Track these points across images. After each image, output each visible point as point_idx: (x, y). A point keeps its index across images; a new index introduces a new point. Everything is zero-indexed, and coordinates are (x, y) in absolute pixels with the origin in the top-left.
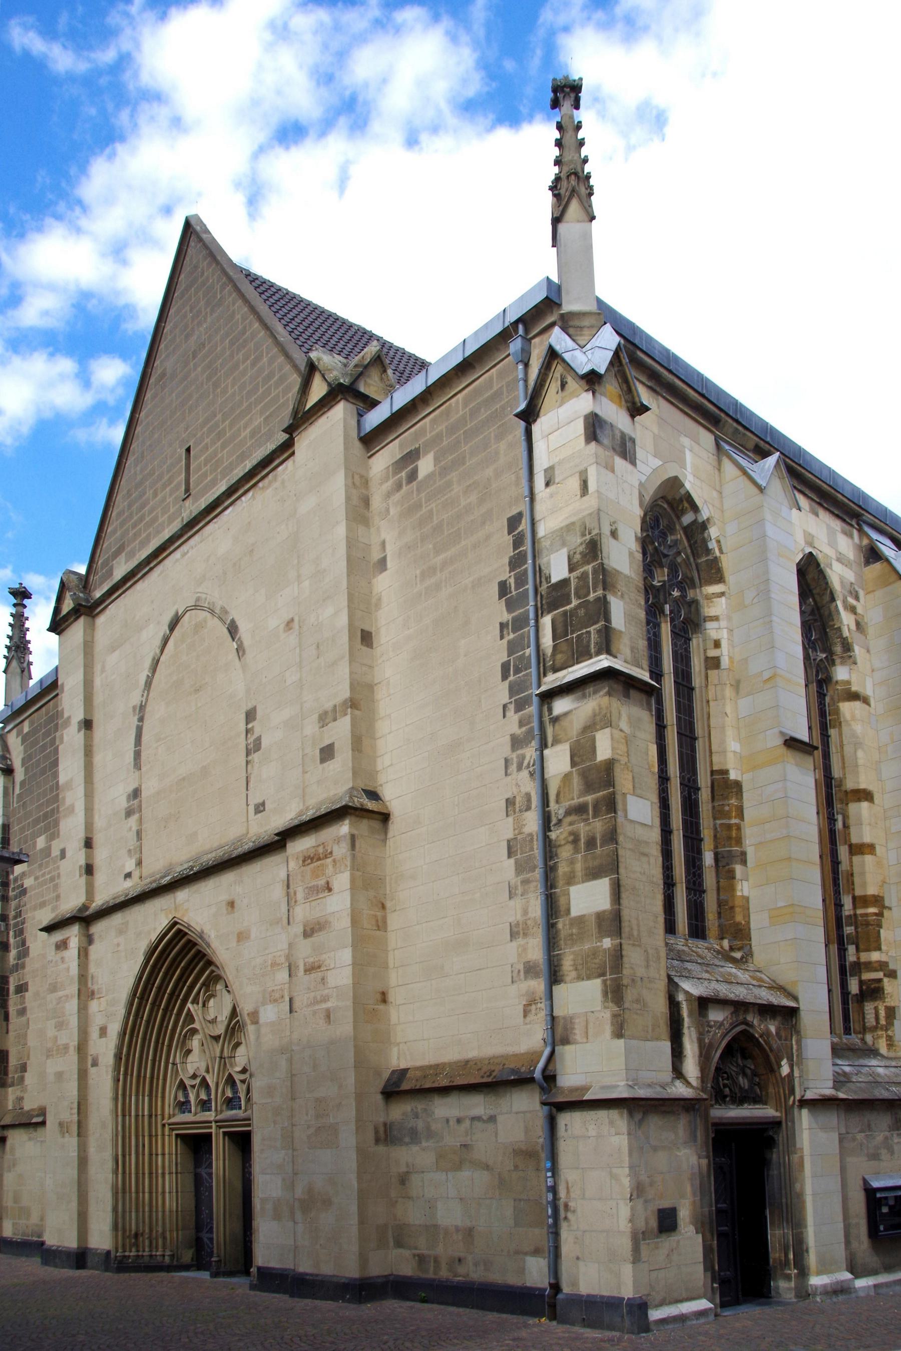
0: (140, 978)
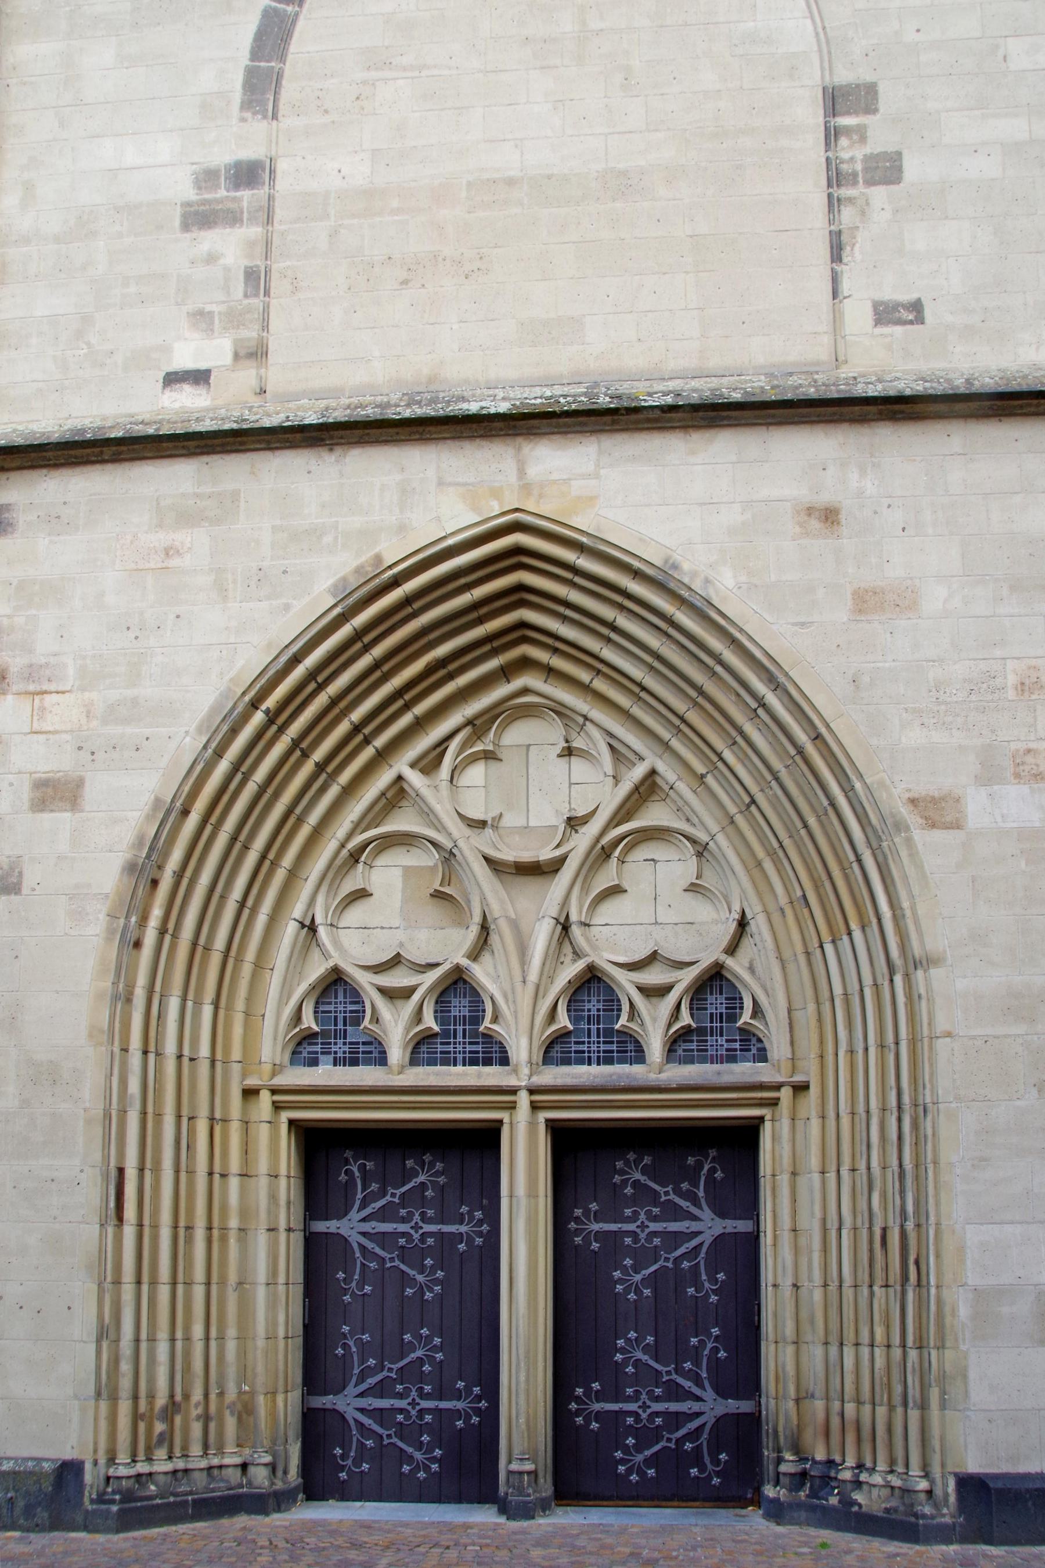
0: (296, 660)
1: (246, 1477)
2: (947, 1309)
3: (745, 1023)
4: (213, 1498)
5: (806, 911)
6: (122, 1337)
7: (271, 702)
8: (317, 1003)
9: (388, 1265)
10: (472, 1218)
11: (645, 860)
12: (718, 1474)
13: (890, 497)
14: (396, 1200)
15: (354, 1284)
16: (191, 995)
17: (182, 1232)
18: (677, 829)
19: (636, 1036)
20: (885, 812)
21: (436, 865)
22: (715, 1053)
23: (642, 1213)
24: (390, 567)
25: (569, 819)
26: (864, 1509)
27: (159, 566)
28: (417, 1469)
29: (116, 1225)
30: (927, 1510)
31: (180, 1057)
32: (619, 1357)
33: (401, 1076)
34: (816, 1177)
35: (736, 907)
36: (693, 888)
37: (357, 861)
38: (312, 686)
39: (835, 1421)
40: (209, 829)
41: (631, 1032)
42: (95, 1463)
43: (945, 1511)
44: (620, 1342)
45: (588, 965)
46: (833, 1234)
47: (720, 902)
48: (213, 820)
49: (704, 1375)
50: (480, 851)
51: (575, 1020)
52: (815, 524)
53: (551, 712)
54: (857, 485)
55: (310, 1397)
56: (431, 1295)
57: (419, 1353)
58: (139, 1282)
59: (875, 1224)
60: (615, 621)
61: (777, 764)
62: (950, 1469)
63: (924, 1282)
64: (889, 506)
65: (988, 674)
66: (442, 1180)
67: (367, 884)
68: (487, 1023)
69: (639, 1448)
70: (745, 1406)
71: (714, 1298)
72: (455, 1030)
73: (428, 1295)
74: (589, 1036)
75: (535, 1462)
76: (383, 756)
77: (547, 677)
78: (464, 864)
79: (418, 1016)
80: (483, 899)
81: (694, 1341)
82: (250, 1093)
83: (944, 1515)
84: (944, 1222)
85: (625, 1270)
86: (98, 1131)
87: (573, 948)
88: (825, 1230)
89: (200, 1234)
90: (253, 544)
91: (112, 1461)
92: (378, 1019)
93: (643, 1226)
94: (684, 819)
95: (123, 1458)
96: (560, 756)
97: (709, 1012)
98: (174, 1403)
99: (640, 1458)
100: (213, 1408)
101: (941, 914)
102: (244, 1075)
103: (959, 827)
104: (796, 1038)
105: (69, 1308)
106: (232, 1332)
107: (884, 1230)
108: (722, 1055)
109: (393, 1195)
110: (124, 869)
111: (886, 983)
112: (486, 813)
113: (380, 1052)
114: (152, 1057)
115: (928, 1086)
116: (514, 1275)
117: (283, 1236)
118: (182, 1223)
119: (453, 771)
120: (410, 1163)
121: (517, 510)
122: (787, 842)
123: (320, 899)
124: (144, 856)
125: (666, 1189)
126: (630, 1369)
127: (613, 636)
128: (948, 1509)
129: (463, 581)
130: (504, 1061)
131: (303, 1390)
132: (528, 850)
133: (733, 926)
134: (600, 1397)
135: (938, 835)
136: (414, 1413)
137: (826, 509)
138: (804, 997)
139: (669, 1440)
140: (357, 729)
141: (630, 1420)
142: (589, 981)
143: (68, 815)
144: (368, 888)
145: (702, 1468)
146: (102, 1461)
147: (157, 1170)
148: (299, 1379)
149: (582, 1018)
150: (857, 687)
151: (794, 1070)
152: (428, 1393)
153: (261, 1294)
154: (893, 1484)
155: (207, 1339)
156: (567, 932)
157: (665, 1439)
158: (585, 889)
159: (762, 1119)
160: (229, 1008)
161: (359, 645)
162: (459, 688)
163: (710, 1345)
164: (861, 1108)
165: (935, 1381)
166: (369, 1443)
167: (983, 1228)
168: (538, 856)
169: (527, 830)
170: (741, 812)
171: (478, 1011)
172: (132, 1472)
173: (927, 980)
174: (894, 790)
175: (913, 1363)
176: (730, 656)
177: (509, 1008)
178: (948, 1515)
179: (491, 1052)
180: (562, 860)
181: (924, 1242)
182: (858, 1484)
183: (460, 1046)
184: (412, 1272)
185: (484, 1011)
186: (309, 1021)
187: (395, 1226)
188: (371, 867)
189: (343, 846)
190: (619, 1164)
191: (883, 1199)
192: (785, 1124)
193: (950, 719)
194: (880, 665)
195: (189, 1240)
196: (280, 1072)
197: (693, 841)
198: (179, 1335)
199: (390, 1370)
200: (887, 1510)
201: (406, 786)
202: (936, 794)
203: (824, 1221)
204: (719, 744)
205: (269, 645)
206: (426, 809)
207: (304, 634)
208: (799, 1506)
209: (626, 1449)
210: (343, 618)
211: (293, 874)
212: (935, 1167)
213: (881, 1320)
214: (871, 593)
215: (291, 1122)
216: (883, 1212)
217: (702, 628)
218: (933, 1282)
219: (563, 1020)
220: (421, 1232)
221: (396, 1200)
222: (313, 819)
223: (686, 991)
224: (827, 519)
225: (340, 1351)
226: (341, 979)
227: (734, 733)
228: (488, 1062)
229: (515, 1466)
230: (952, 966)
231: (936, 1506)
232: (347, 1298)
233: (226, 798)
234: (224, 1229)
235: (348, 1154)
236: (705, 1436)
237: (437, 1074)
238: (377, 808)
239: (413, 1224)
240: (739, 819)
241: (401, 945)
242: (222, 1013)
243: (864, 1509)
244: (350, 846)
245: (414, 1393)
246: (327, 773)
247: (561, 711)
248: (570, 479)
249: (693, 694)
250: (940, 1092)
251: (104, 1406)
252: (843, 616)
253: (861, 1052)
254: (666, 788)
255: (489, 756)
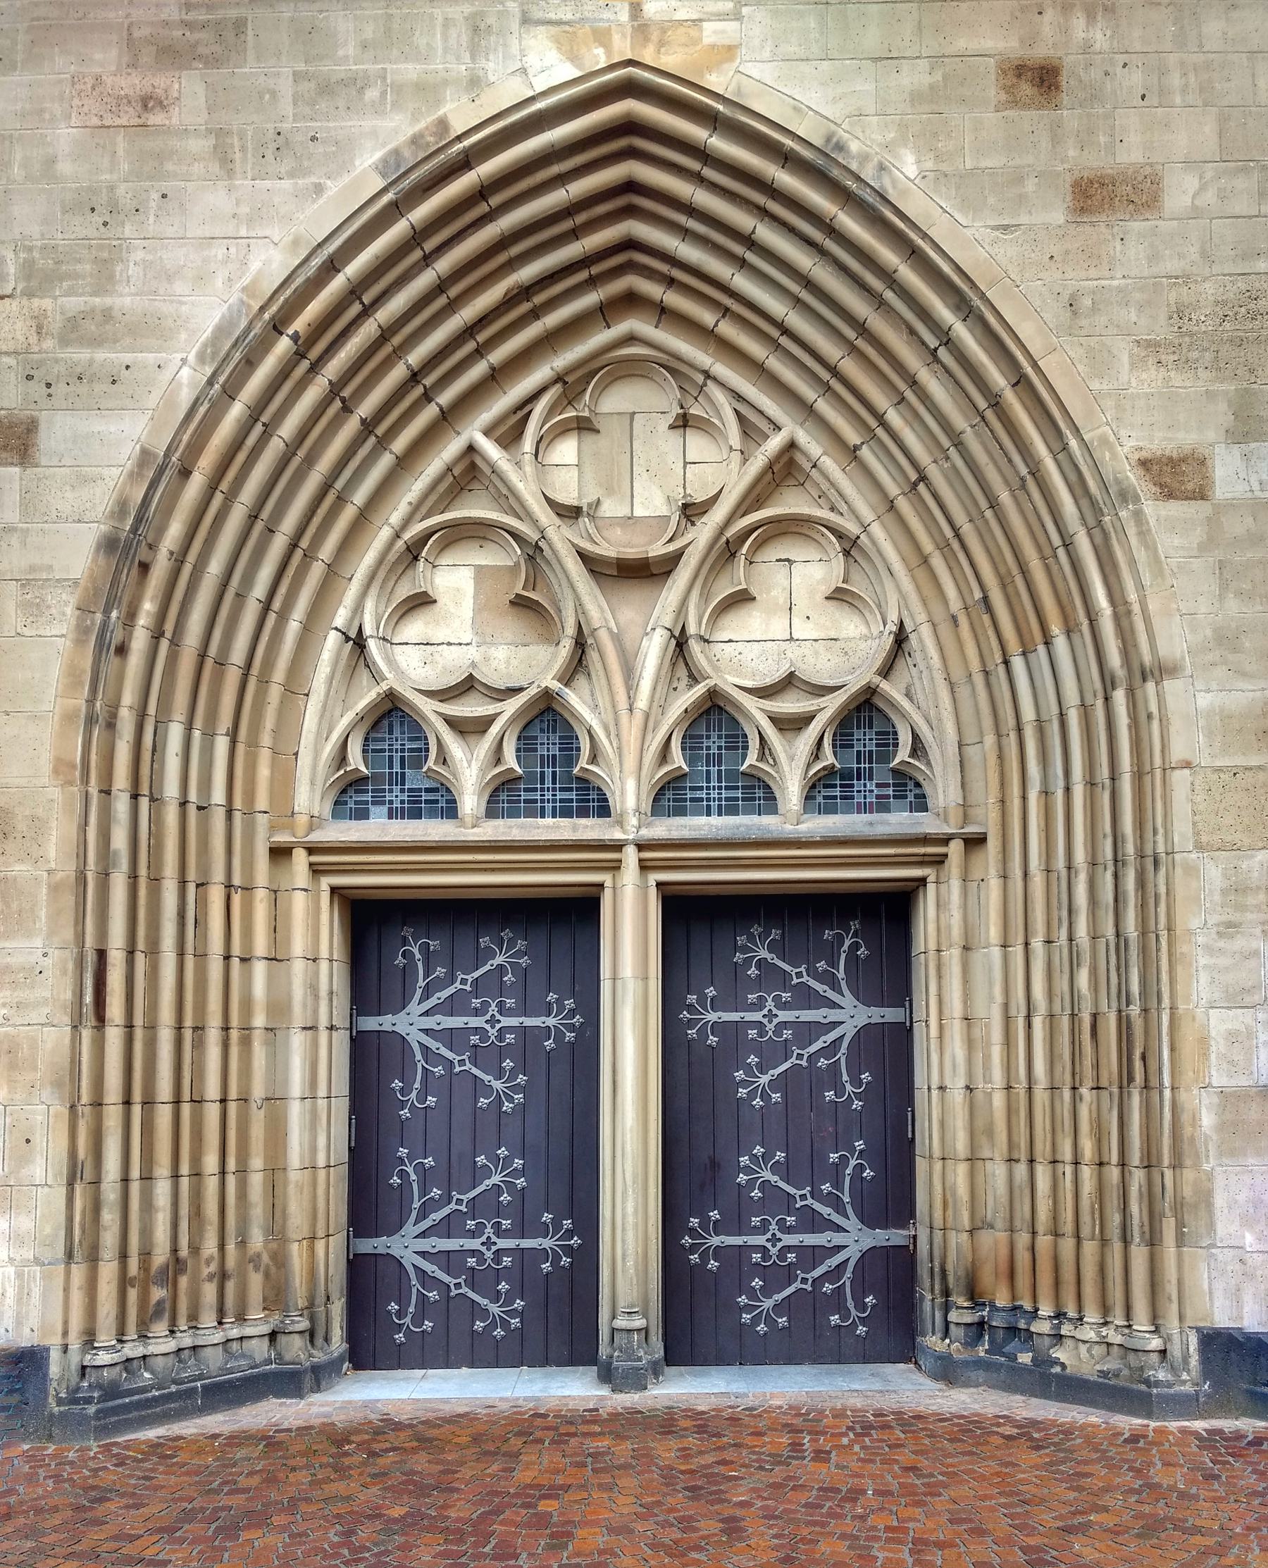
0: (332, 267)
1: (275, 1349)
2: (1185, 1118)
3: (903, 762)
4: (229, 1382)
5: (986, 618)
6: (103, 1176)
7: (300, 324)
8: (366, 739)
9: (458, 1069)
10: (561, 1008)
11: (777, 561)
12: (863, 1321)
13: (1127, 52)
14: (468, 988)
15: (413, 1095)
16: (198, 722)
17: (188, 1034)
18: (820, 518)
19: (766, 779)
20: (1109, 477)
21: (517, 564)
22: (863, 800)
23: (770, 1000)
24: (459, 138)
25: (685, 506)
26: (1068, 1371)
27: (136, 121)
28: (493, 1326)
29: (94, 1027)
30: (1162, 1375)
31: (184, 804)
32: (742, 1178)
33: (476, 830)
34: (996, 952)
35: (893, 617)
36: (839, 596)
37: (416, 558)
38: (356, 308)
39: (1023, 1258)
40: (218, 499)
41: (761, 775)
42: (65, 1349)
43: (1185, 1376)
44: (744, 1160)
45: (709, 690)
46: (1021, 1023)
47: (872, 611)
48: (224, 486)
49: (847, 1199)
50: (573, 545)
51: (691, 761)
52: (1026, 89)
53: (661, 369)
54: (1083, 35)
55: (357, 1240)
56: (511, 1105)
57: (496, 1179)
58: (127, 1103)
59: (1083, 1009)
60: (753, 232)
61: (959, 421)
62: (1189, 1323)
63: (1154, 1082)
64: (1125, 65)
65: (1248, 294)
66: (524, 961)
67: (429, 585)
68: (583, 762)
69: (767, 1291)
70: (896, 1237)
71: (857, 1104)
72: (542, 773)
73: (507, 1106)
74: (708, 781)
75: (645, 1316)
76: (448, 418)
77: (659, 321)
78: (554, 562)
79: (497, 755)
80: (579, 606)
81: (834, 1157)
82: (280, 853)
83: (1184, 1382)
84: (1182, 1007)
85: (748, 1069)
86: (69, 900)
87: (689, 670)
88: (1007, 1019)
89: (213, 1036)
90: (267, 96)
91: (89, 1341)
92: (445, 759)
93: (770, 1016)
94: (827, 507)
95: (105, 1337)
96: (672, 427)
97: (855, 749)
98: (177, 1260)
99: (768, 1304)
100: (231, 1263)
101: (1178, 610)
102: (273, 829)
103: (1203, 497)
104: (967, 779)
105: (28, 1141)
106: (257, 1162)
107: (1095, 1016)
108: (871, 803)
109: (464, 982)
110: (98, 550)
111: (1100, 703)
112: (580, 497)
113: (448, 802)
114: (144, 803)
115: (1161, 831)
116: (619, 1078)
117: (323, 1036)
118: (188, 1022)
119: (538, 443)
120: (484, 941)
121: (630, 63)
122: (967, 529)
123: (370, 605)
124: (128, 528)
125: (798, 970)
126: (756, 1193)
127: (750, 257)
128: (1189, 1375)
129: (555, 169)
130: (604, 810)
131: (348, 1231)
132: (632, 547)
133: (888, 641)
134: (719, 1229)
135: (1175, 508)
136: (489, 1255)
137: (1042, 68)
138: (980, 727)
139: (804, 1281)
140: (415, 377)
141: (756, 1257)
142: (707, 712)
143: (17, 470)
144: (430, 593)
145: (845, 1315)
146: (75, 1345)
147: (154, 951)
148: (344, 1219)
149: (699, 758)
150: (1075, 313)
151: (966, 819)
152: (506, 1230)
153: (296, 1113)
154: (1110, 1340)
155: (223, 1172)
156: (681, 650)
157: (799, 1279)
158: (705, 597)
159: (923, 881)
160: (253, 743)
161: (417, 254)
162: (546, 331)
163: (853, 1162)
164: (1060, 863)
165: (1171, 1209)
166: (433, 1295)
167: (1231, 1013)
168: (647, 552)
169: (631, 522)
170: (904, 494)
171: (571, 749)
172: (116, 1357)
173: (1160, 697)
174: (1120, 448)
175: (1140, 1187)
176: (908, 275)
177: (611, 744)
178: (1189, 1380)
179: (588, 801)
180: (674, 559)
181: (1154, 1032)
182: (1058, 1338)
183: (550, 795)
184: (486, 1078)
185: (578, 749)
186: (356, 760)
187: (465, 1019)
188: (434, 567)
189: (397, 536)
190: (741, 940)
191: (1093, 978)
192: (955, 884)
193: (1195, 354)
194: (1104, 283)
195: (199, 1044)
196: (320, 827)
197: (840, 535)
198: (185, 1169)
199: (459, 1202)
200: (1103, 1374)
201: (479, 462)
202: (1175, 455)
203: (1006, 1006)
204: (880, 399)
205: (296, 243)
206: (505, 491)
207: (345, 227)
208: (979, 1364)
209: (752, 1294)
210: (396, 210)
211: (333, 573)
212: (1169, 935)
213: (1091, 1130)
214: (1096, 186)
215: (334, 890)
216: (1093, 995)
217: (874, 236)
218: (1167, 1081)
219: (678, 760)
220: (498, 1026)
221: (468, 988)
222: (360, 496)
223: (830, 722)
224: (1042, 81)
225: (396, 1180)
226: (397, 709)
227: (902, 386)
228: (583, 813)
229: (621, 1323)
230: (1192, 676)
231: (1173, 1369)
232: (405, 1113)
233: (241, 457)
234: (247, 1029)
235: (407, 932)
236: (848, 1274)
237: (521, 827)
238: (442, 488)
239: (488, 1017)
240: (903, 505)
241: (473, 665)
242: (241, 749)
243: (1068, 1371)
244: (407, 536)
245: (489, 1230)
246: (377, 436)
247: (675, 368)
248: (701, 20)
249: (850, 334)
250: (1176, 839)
251: (78, 1273)
252: (1058, 216)
253: (1060, 794)
254: (807, 466)
255: (584, 426)
